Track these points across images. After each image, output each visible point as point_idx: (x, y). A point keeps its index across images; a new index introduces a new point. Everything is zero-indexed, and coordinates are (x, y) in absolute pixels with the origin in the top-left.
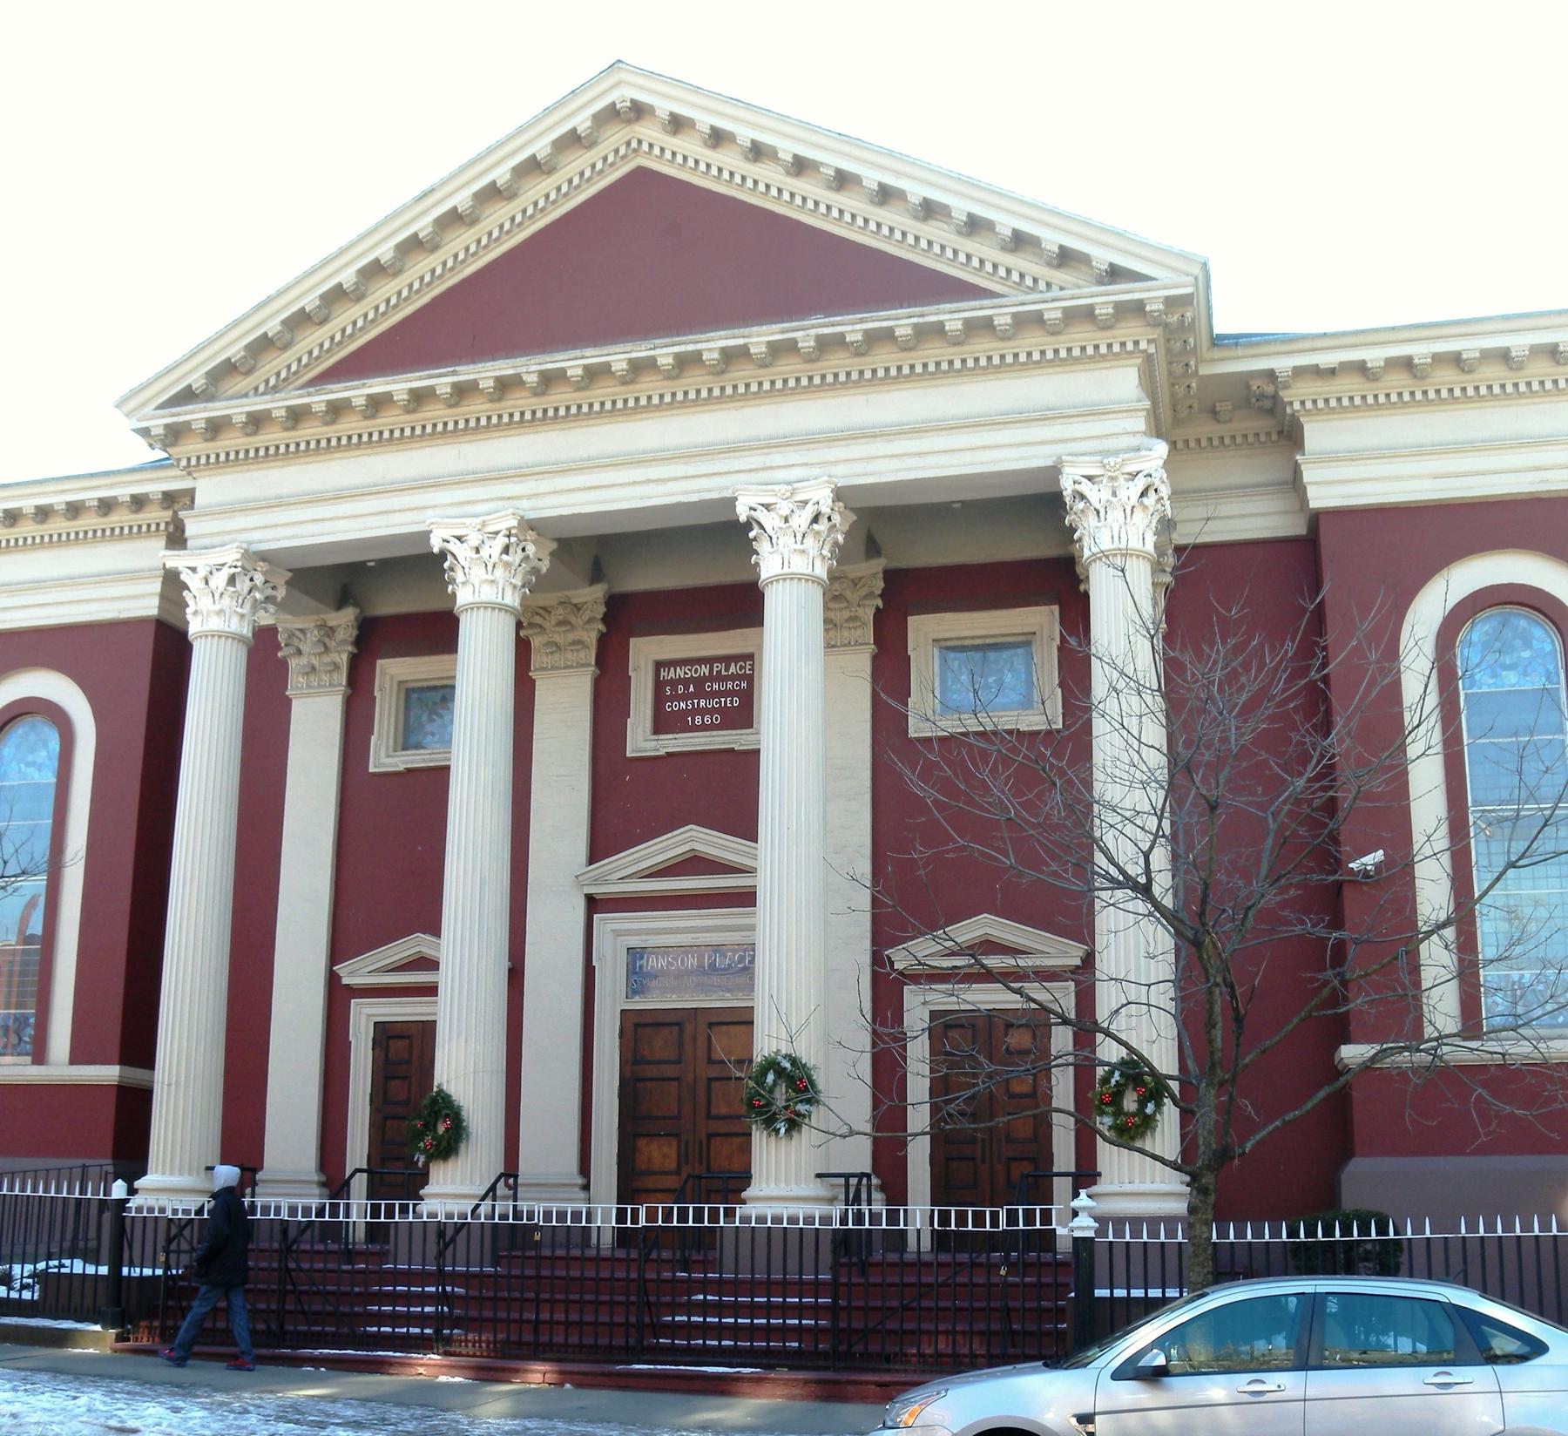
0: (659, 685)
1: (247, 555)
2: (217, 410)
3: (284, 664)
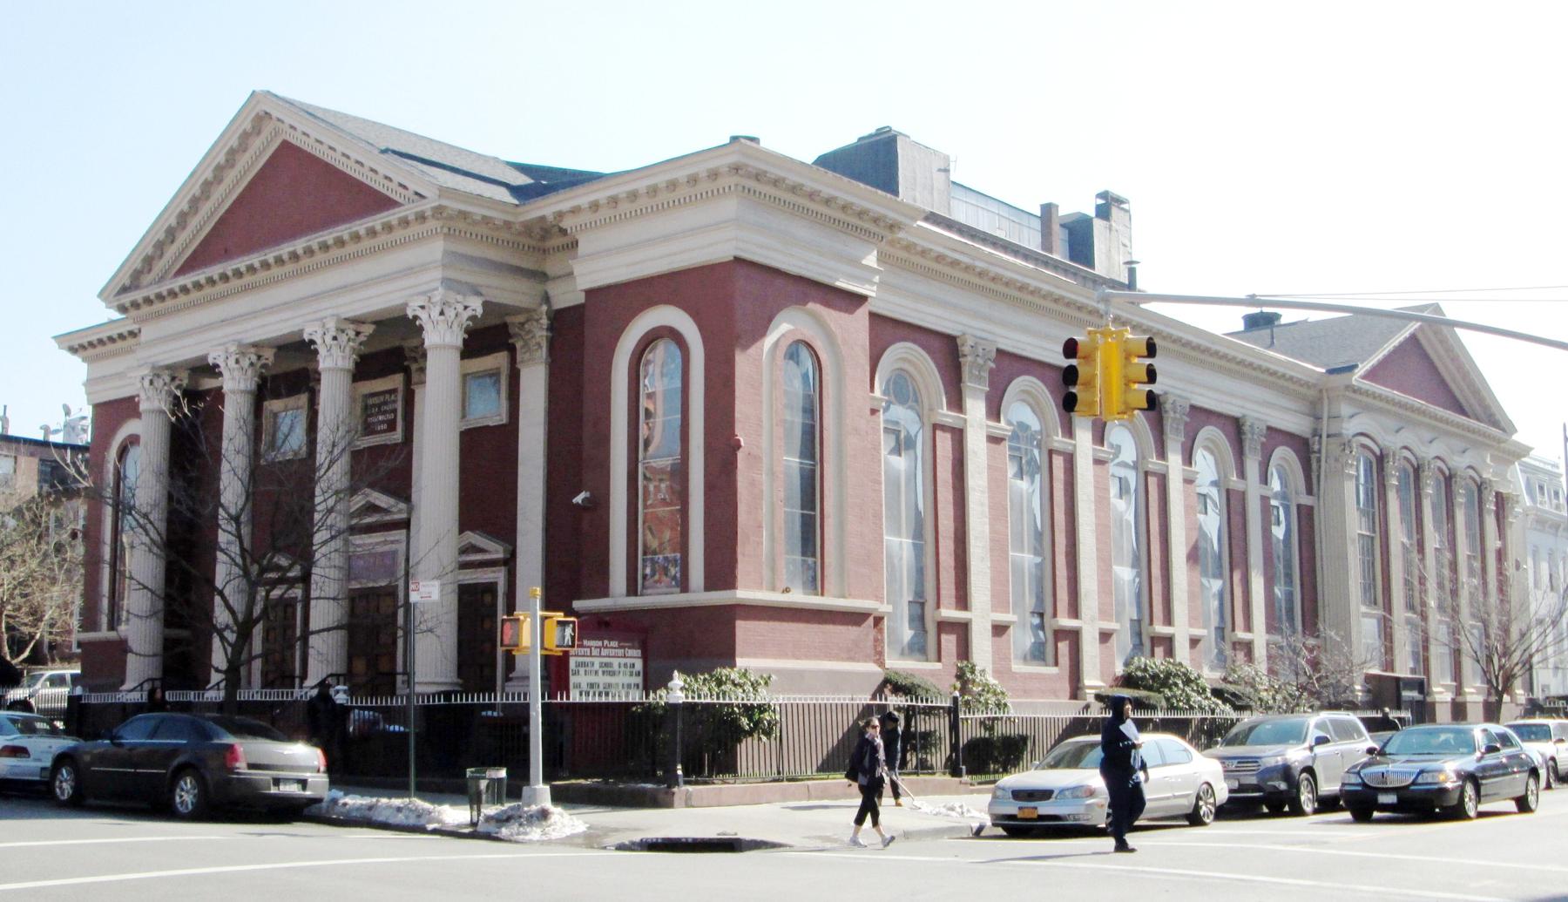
1: (153, 368)
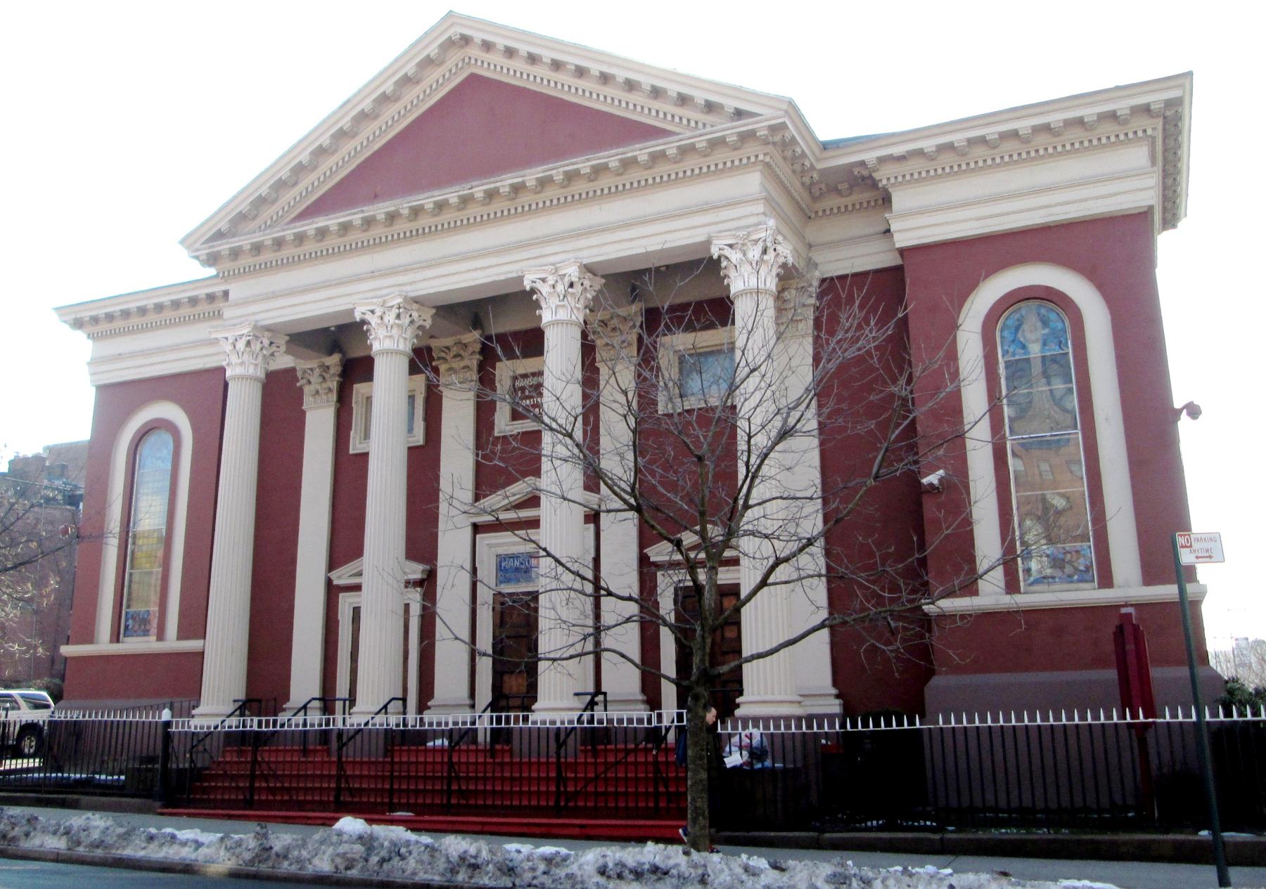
0: (515, 390)
1: (255, 327)
2: (234, 242)
3: (301, 390)
